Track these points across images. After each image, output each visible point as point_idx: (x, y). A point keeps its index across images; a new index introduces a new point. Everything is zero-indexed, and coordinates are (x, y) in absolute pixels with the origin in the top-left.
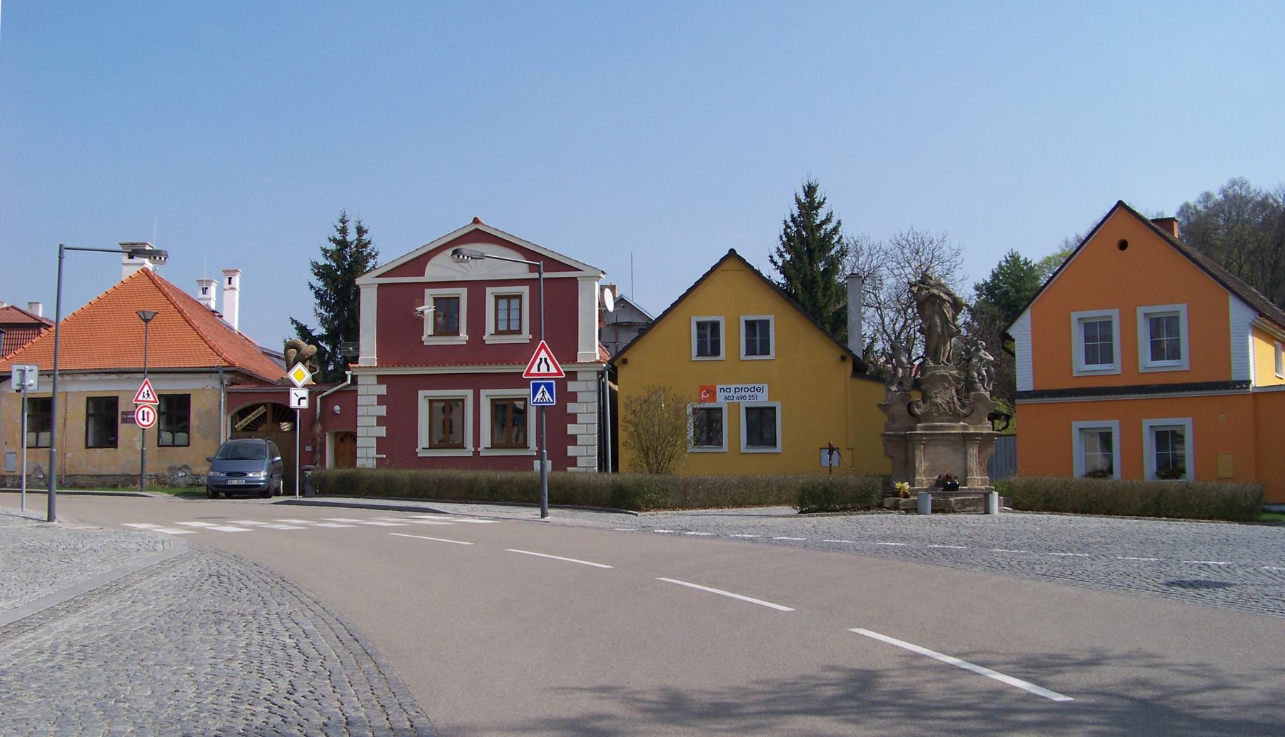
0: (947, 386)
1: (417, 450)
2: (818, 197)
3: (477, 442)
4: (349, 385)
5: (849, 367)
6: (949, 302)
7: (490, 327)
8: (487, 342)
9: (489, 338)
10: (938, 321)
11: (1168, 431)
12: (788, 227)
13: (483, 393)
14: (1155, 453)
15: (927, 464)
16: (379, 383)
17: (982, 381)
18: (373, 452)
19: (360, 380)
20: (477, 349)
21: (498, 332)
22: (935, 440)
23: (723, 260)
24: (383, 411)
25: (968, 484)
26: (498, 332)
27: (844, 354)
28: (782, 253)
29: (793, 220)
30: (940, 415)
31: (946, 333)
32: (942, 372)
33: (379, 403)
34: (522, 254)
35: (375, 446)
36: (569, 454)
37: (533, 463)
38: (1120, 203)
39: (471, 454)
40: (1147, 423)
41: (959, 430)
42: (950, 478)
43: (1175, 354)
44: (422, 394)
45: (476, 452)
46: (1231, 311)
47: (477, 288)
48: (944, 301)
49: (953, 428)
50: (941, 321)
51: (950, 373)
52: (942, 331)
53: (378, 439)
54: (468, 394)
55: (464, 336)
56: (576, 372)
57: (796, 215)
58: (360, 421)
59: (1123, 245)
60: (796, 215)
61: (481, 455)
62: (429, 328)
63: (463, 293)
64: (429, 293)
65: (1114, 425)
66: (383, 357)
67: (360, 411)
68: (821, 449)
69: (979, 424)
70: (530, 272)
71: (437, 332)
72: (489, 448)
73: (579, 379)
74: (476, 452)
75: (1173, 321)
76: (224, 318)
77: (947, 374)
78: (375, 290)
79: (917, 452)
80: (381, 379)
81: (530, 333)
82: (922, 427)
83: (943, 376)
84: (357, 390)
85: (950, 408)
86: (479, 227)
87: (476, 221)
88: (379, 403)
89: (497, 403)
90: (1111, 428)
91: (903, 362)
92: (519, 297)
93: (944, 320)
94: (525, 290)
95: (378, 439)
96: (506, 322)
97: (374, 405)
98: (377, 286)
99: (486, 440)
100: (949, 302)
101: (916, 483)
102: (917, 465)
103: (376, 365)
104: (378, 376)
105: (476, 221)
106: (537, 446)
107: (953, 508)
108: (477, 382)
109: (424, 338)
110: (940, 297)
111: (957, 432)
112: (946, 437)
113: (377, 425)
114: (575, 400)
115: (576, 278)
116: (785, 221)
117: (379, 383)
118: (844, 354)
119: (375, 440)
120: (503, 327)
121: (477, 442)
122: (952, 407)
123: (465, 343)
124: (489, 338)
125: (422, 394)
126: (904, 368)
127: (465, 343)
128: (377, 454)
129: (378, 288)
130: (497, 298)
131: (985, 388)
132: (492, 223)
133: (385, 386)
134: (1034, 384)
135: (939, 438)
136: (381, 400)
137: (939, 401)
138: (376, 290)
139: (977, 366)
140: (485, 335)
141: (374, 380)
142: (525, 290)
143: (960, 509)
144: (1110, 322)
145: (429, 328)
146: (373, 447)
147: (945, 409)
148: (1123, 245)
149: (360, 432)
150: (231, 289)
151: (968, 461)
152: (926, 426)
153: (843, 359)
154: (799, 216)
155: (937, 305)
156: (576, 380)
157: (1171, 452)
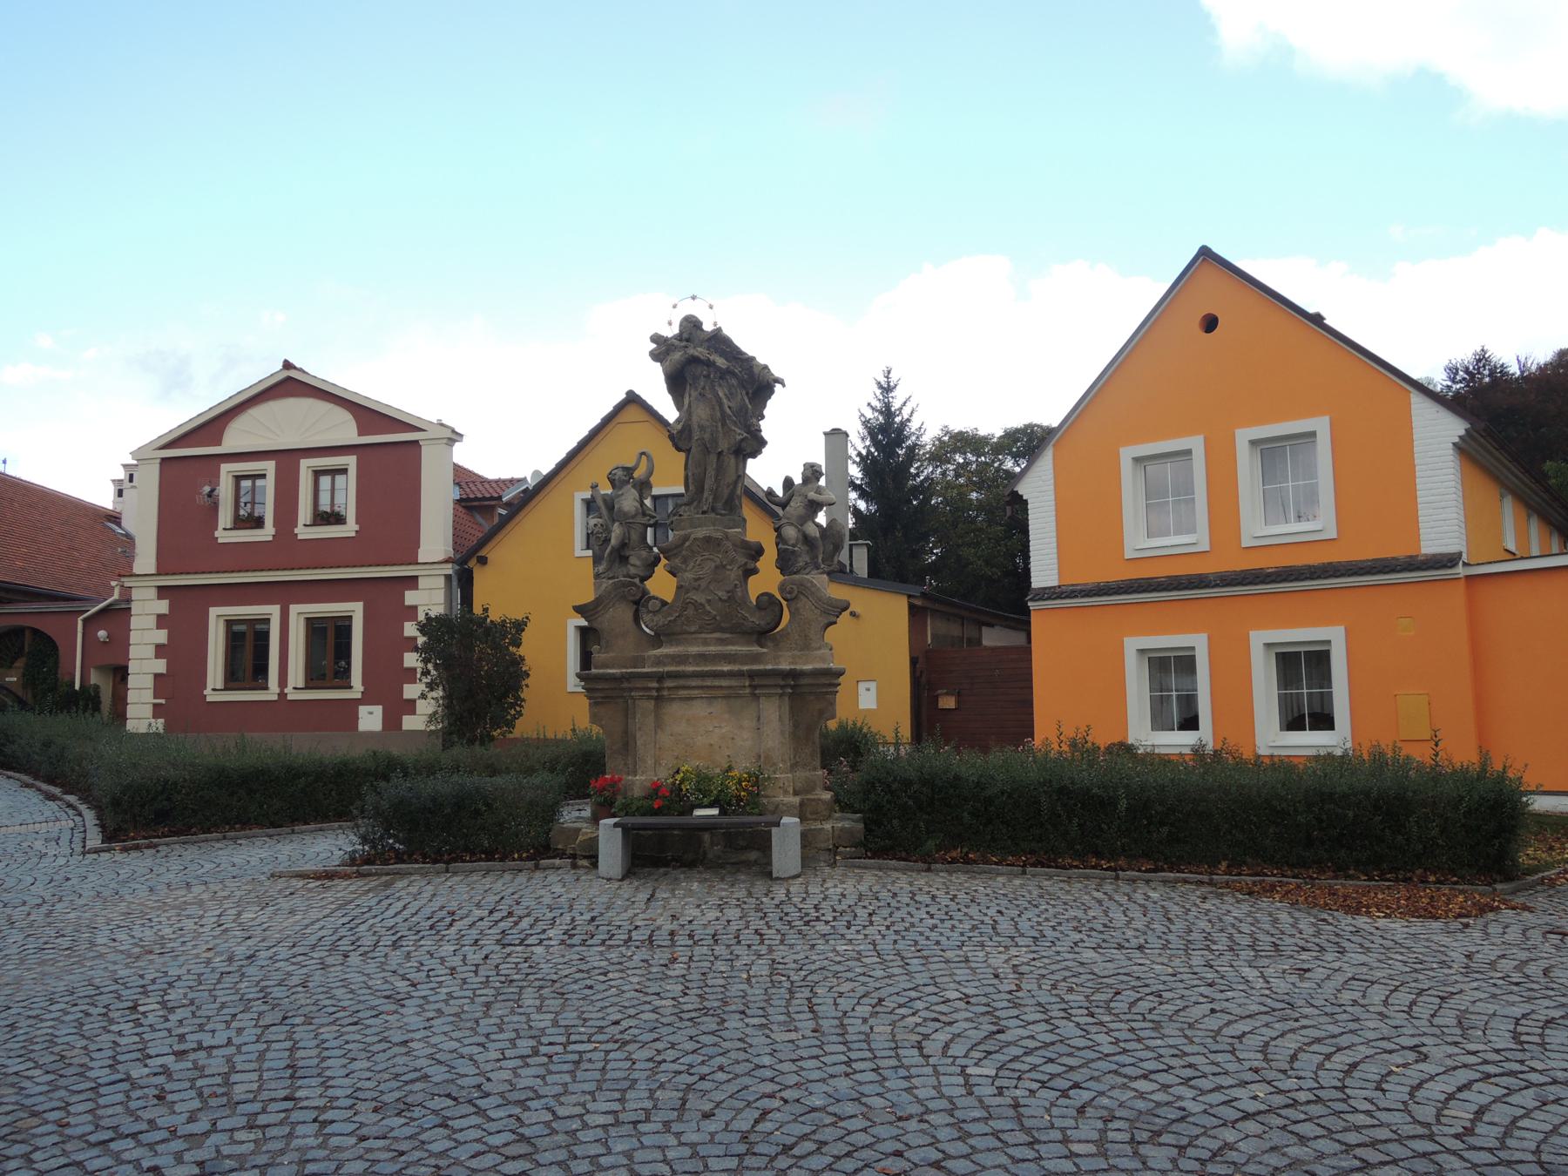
1: (205, 692)
2: (894, 377)
3: (283, 681)
4: (116, 601)
9: (304, 532)
11: (1300, 652)
13: (295, 609)
14: (1275, 692)
16: (160, 597)
18: (148, 696)
19: (135, 594)
20: (286, 549)
23: (619, 408)
36: (406, 696)
38: (1205, 254)
39: (275, 698)
40: (1259, 639)
42: (858, 753)
43: (1324, 721)
44: (214, 612)
45: (282, 695)
46: (1417, 421)
47: (287, 458)
53: (157, 676)
54: (273, 611)
56: (417, 577)
58: (133, 652)
59: (1210, 324)
63: (269, 466)
64: (227, 470)
65: (1199, 643)
67: (134, 637)
73: (420, 587)
74: (282, 695)
75: (1319, 660)
76: (124, 523)
78: (157, 467)
80: (163, 592)
86: (293, 374)
89: (236, 628)
90: (1193, 648)
92: (344, 471)
94: (351, 461)
95: (157, 676)
98: (158, 461)
99: (296, 674)
104: (159, 587)
106: (363, 685)
108: (285, 593)
114: (160, 617)
115: (417, 442)
119: (151, 678)
121: (283, 681)
124: (304, 532)
125: (214, 612)
129: (161, 464)
130: (318, 474)
132: (320, 367)
133: (167, 601)
134: (1060, 573)
136: (161, 621)
138: (158, 465)
140: (296, 526)
141: (153, 593)
142: (351, 461)
145: (225, 517)
148: (1210, 324)
149: (133, 667)
150: (132, 487)
156: (417, 589)
157: (1305, 691)
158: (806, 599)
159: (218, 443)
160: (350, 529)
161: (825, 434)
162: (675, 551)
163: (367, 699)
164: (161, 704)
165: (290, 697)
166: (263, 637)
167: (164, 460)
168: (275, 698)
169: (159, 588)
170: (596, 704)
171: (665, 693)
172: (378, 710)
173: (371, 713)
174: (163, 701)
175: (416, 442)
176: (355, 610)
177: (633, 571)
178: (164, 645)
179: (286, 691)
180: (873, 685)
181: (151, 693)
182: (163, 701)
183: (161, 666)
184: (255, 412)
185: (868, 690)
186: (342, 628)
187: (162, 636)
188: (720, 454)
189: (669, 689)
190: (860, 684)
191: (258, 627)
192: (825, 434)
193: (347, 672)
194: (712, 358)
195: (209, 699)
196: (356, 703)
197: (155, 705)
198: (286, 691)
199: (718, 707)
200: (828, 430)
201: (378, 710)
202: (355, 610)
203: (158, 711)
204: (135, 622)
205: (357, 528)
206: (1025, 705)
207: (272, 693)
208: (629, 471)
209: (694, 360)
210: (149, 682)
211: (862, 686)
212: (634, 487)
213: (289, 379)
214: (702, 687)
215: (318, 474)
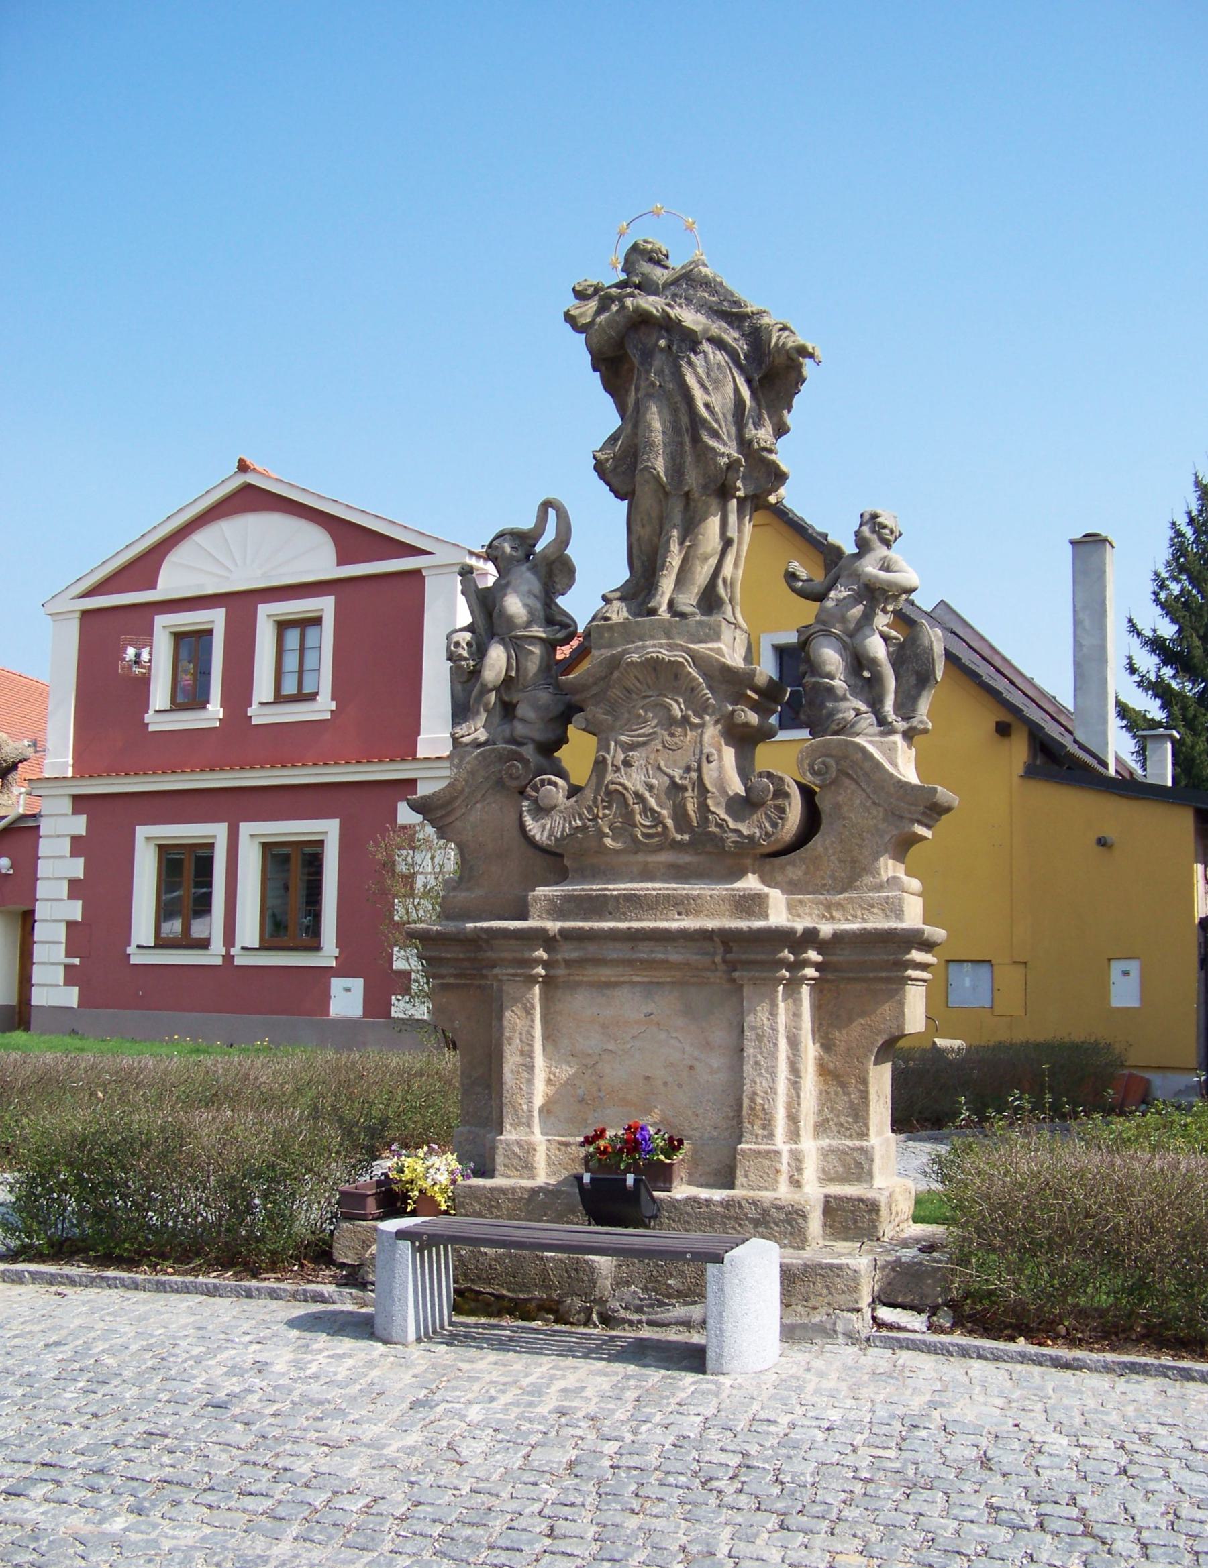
0: (677, 712)
1: (129, 950)
5: (1019, 751)
6: (719, 343)
7: (263, 688)
8: (255, 721)
9: (259, 715)
10: (657, 425)
12: (1179, 534)
13: (246, 828)
15: (566, 1071)
16: (76, 811)
17: (870, 688)
21: (280, 698)
22: (598, 962)
24: (77, 869)
25: (740, 1179)
26: (280, 698)
27: (1006, 717)
28: (1163, 581)
29: (1191, 521)
30: (636, 846)
31: (693, 479)
32: (658, 649)
33: (74, 853)
34: (321, 525)
35: (64, 940)
37: (329, 982)
41: (712, 915)
44: (143, 832)
45: (228, 958)
48: (690, 340)
49: (681, 905)
50: (674, 429)
51: (688, 651)
52: (676, 468)
53: (71, 925)
54: (217, 832)
55: (215, 710)
57: (1194, 513)
60: (1194, 513)
61: (236, 963)
62: (160, 696)
64: (164, 624)
66: (84, 764)
67: (43, 868)
68: (948, 961)
69: (847, 885)
70: (339, 564)
71: (177, 705)
72: (150, 947)
74: (228, 958)
77: (678, 656)
79: (512, 1018)
80: (81, 803)
81: (332, 699)
82: (550, 900)
83: (655, 665)
84: (38, 827)
85: (680, 815)
87: (243, 467)
88: (74, 853)
89: (276, 851)
91: (509, 621)
92: (317, 621)
93: (685, 420)
94: (325, 605)
95: (71, 925)
96: (296, 675)
97: (63, 857)
98: (78, 615)
99: (249, 929)
100: (719, 343)
101: (500, 1159)
102: (508, 1076)
103: (70, 774)
105: (243, 467)
107: (601, 1301)
109: (149, 717)
110: (669, 326)
111: (710, 924)
112: (644, 952)
113: (69, 898)
116: (1174, 524)
117: (76, 811)
118: (1006, 717)
120: (290, 688)
122: (691, 807)
123: (218, 724)
124: (259, 715)
125: (143, 832)
126: (515, 644)
127: (218, 724)
128: (67, 956)
130: (283, 626)
131: (882, 721)
135: (613, 952)
137: (634, 780)
139: (843, 620)
141: (67, 805)
142: (325, 605)
143: (639, 1310)
144: (210, 632)
145: (160, 696)
146: (61, 943)
147: (658, 820)
149: (41, 911)
151: (748, 1069)
152: (568, 898)
153: (1003, 730)
154: (1200, 512)
155: (658, 361)
158: (853, 786)
159: (153, 586)
160: (323, 707)
161: (1073, 542)
162: (594, 690)
163: (342, 970)
164: (74, 966)
165: (237, 962)
166: (204, 864)
167: (85, 614)
168: (219, 962)
169: (77, 799)
170: (445, 987)
171: (561, 972)
172: (358, 984)
173: (348, 990)
174: (77, 961)
175: (417, 574)
176: (328, 830)
177: (520, 729)
178: (80, 880)
179: (233, 951)
180: (1133, 967)
181: (62, 948)
182: (77, 961)
183: (75, 911)
184: (200, 537)
185: (1126, 974)
186: (311, 855)
187: (77, 869)
188: (687, 494)
189: (568, 963)
190: (1114, 964)
191: (200, 853)
192: (1073, 542)
193: (314, 930)
194: (673, 313)
195: (133, 960)
196: (327, 972)
197: (68, 967)
198: (233, 951)
199: (664, 1004)
200: (1078, 535)
201: (358, 984)
202: (328, 830)
203: (71, 974)
204: (44, 847)
205: (333, 705)
206: (894, 1080)
207: (213, 956)
208: (524, 540)
209: (643, 320)
210: (61, 933)
211: (1117, 968)
212: (534, 569)
213: (248, 486)
214: (629, 963)
215: (283, 626)
